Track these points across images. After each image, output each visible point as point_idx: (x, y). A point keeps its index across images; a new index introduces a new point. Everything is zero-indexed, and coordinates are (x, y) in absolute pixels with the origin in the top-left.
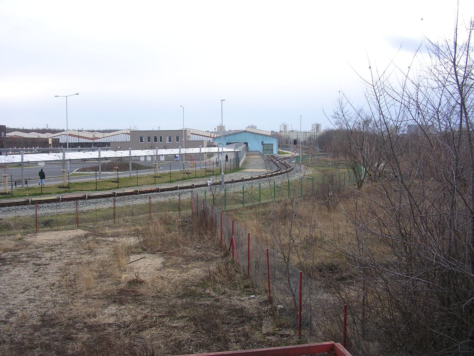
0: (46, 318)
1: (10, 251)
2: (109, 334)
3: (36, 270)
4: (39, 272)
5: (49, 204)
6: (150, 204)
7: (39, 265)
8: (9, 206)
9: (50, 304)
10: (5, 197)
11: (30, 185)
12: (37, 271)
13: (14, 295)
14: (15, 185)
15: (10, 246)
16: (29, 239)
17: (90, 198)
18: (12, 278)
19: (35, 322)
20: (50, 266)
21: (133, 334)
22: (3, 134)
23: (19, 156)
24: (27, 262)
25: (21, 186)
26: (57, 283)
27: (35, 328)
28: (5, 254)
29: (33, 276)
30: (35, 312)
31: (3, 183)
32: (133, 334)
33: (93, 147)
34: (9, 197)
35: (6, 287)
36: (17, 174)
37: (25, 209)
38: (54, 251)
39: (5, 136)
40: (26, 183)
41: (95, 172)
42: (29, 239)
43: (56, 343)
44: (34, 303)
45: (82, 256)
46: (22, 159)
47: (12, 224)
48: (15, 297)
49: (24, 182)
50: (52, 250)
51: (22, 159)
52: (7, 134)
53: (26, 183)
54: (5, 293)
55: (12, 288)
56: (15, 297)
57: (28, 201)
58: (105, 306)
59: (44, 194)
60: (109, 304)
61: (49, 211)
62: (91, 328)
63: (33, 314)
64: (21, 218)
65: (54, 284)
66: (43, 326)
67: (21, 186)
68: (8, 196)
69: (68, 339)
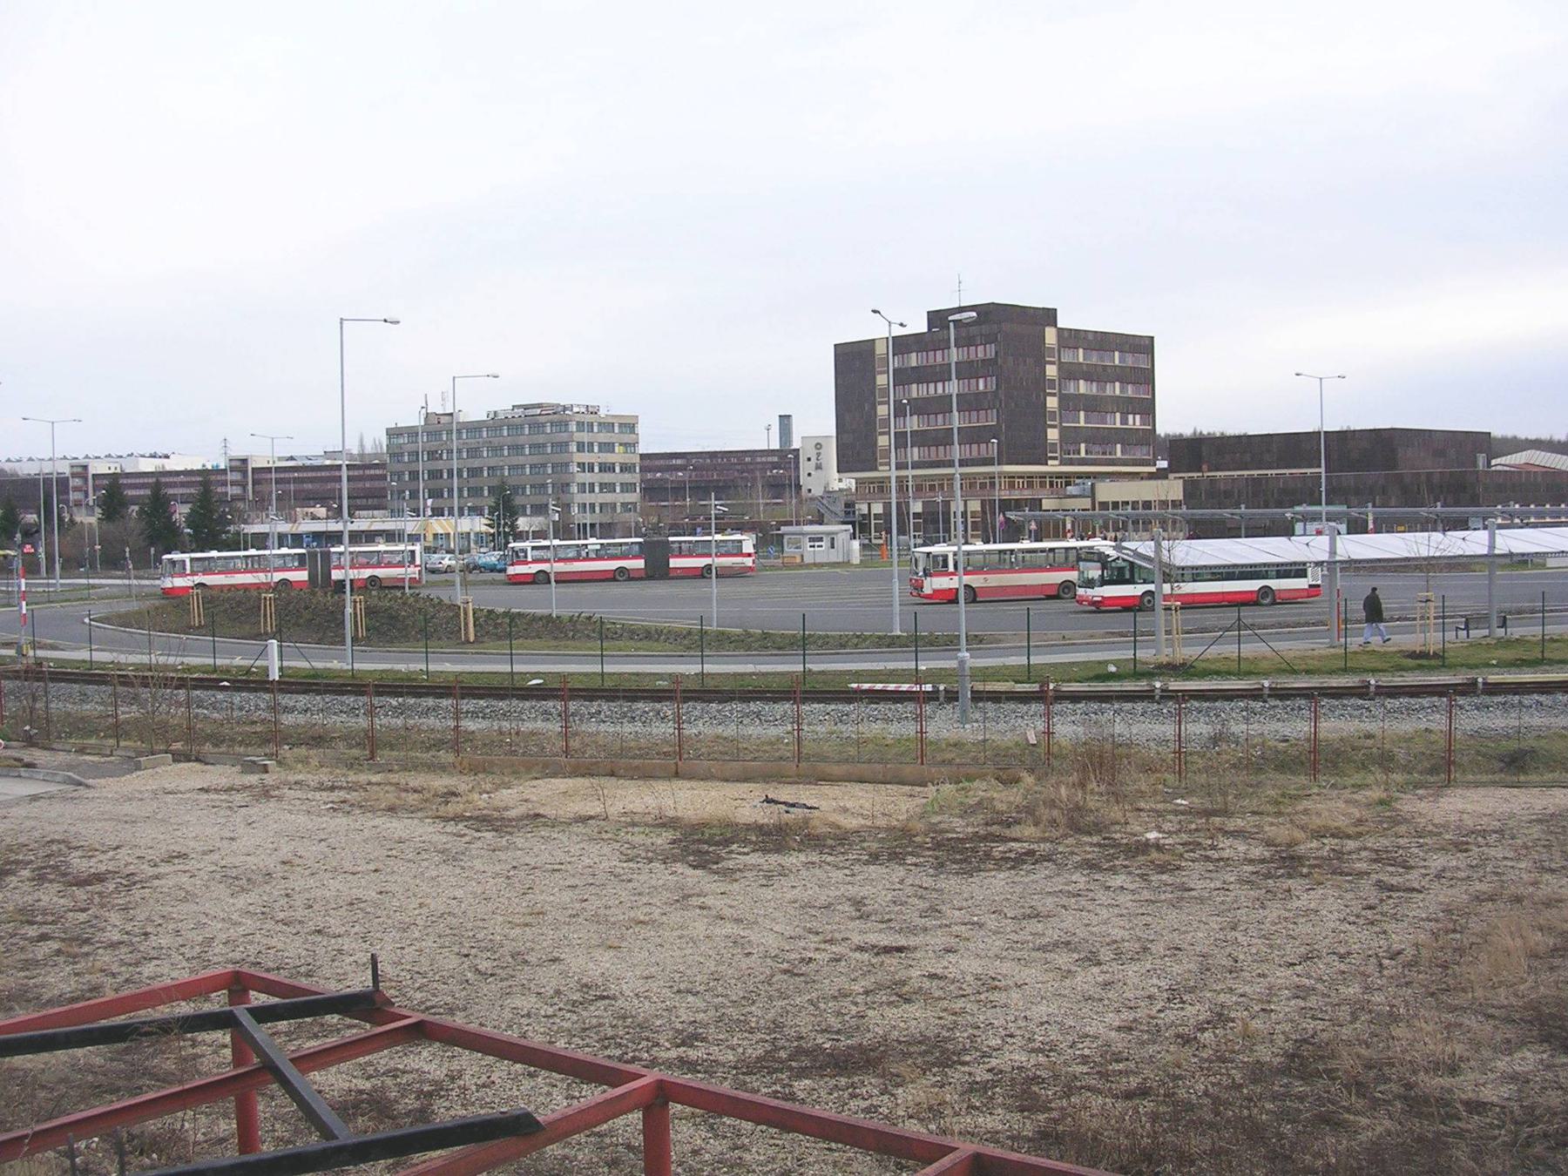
0: (1306, 1051)
1: (1333, 836)
2: (1460, 1134)
3: (1372, 901)
4: (1379, 909)
5: (1542, 698)
6: (1315, 739)
7: (1392, 888)
8: (1412, 695)
9: (1344, 1013)
10: (1420, 667)
11: (1516, 632)
12: (1370, 908)
13: (1264, 968)
14: (1467, 628)
15: (1341, 822)
16: (1409, 804)
17: (1493, 689)
18: (1286, 919)
19: (1264, 1053)
20: (1421, 896)
21: (1538, 1149)
22: (1481, 459)
23: (1483, 535)
24: (1361, 874)
25: (1486, 632)
26: (1410, 952)
27: (1258, 1072)
28: (1315, 844)
29: (1352, 919)
30: (1287, 1027)
31: (1419, 622)
32: (1538, 1149)
33: (1237, 571)
34: (1431, 669)
35: (1254, 941)
36: (1465, 594)
37: (1461, 708)
38: (1466, 851)
39: (1489, 465)
40: (1504, 624)
41: (1034, 660)
42: (1409, 804)
43: (1287, 1128)
44: (1304, 999)
45: (1547, 876)
46: (1492, 546)
47: (1401, 755)
48: (1259, 975)
49: (1495, 622)
50: (1461, 847)
51: (1492, 546)
52: (1493, 462)
53: (1504, 624)
54: (1241, 957)
55: (1271, 946)
56: (1259, 975)
57: (1474, 683)
58: (1509, 1047)
59: (1551, 662)
60: (1522, 1044)
61: (1536, 720)
62: (1416, 1103)
63: (1276, 1028)
64: (1433, 737)
65: (1399, 953)
66: (1284, 1071)
67: (1486, 632)
68: (1433, 662)
69: (1327, 1122)
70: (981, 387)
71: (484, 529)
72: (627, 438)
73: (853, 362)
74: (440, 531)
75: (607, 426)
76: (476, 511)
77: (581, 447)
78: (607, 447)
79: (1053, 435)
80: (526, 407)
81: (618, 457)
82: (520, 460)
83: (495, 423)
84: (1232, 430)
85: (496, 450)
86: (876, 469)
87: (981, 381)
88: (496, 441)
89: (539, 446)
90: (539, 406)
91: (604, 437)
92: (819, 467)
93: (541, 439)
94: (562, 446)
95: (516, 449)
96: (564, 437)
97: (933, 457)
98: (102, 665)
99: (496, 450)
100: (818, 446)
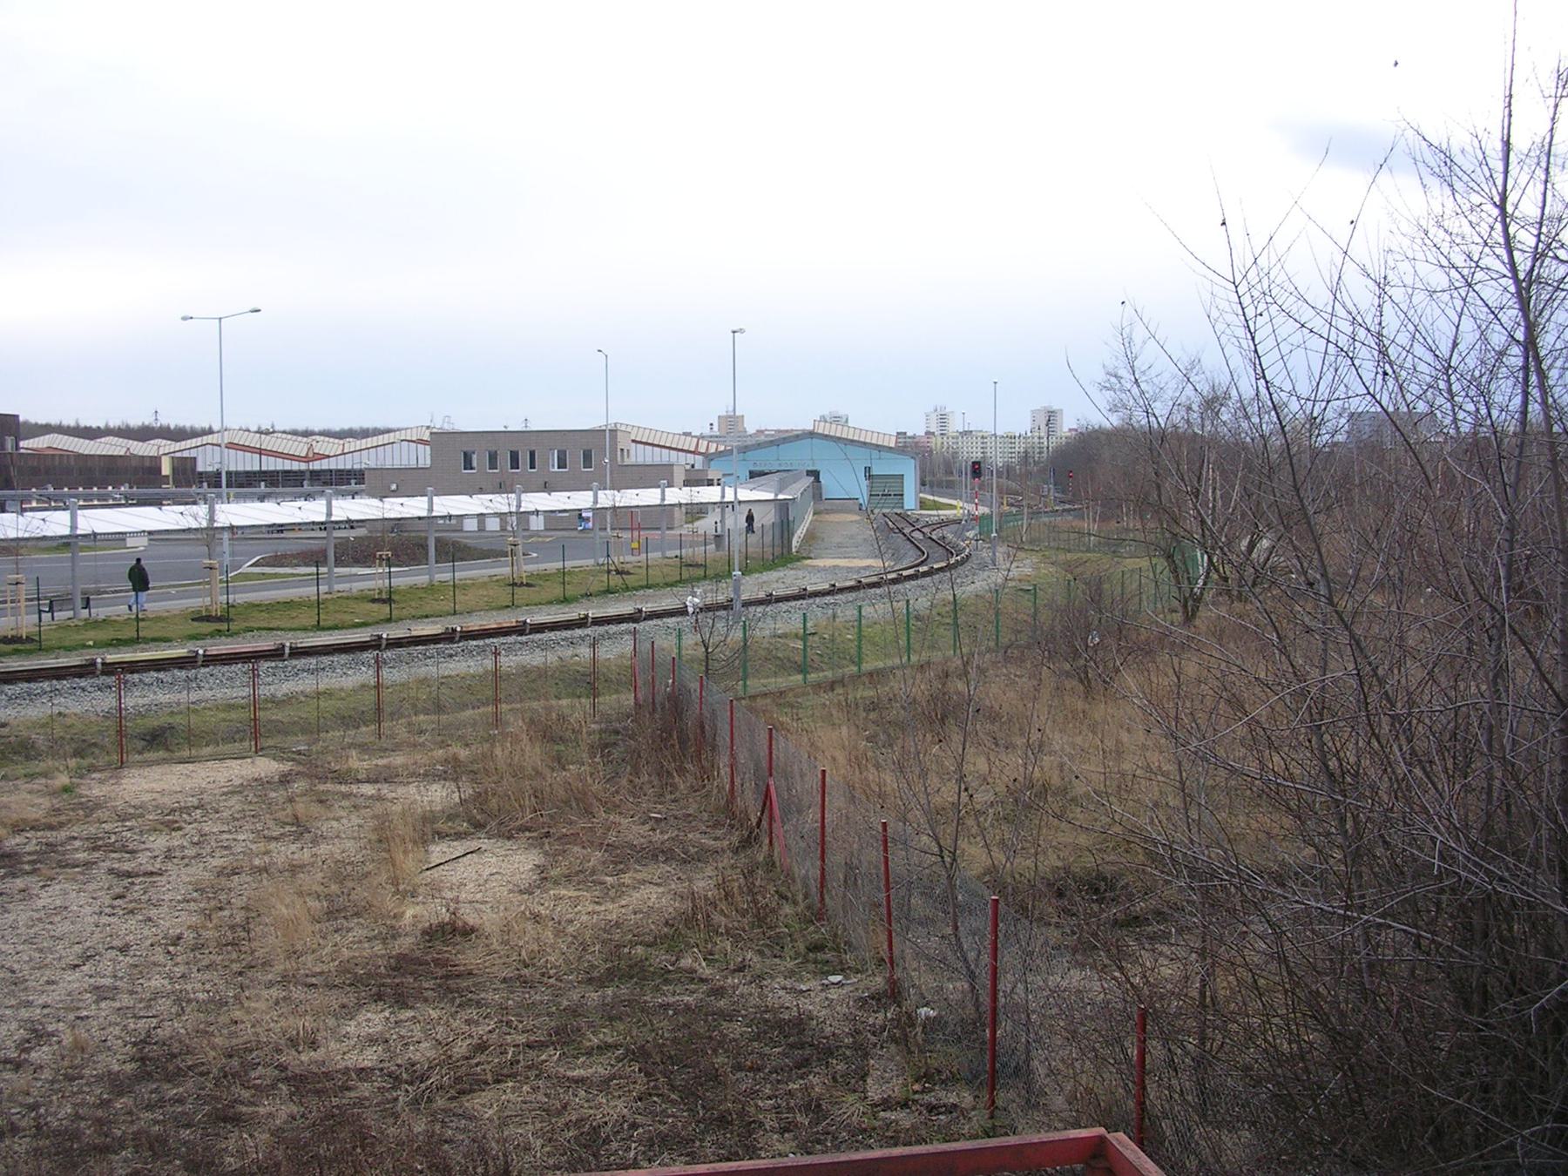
0: (152, 1051)
1: (32, 828)
2: (360, 1103)
3: (118, 890)
4: (129, 897)
5: (161, 675)
6: (496, 674)
7: (129, 875)
8: (28, 680)
9: (164, 1006)
10: (17, 652)
11: (99, 612)
12: (121, 897)
13: (48, 974)
14: (51, 610)
15: (33, 814)
16: (95, 789)
17: (298, 653)
18: (40, 920)
19: (115, 1063)
20: (164, 879)
21: (440, 1102)
22: (9, 442)
23: (64, 517)
24: (88, 864)
25: (71, 614)
26: (189, 936)
27: (117, 1085)
28: (18, 839)
29: (108, 910)
30: (117, 1031)
31: (9, 605)
32: (440, 1102)
34: (29, 652)
35: (20, 948)
36: (55, 574)
37: (83, 690)
38: (180, 829)
39: (17, 448)
40: (87, 605)
42: (95, 789)
43: (185, 1134)
44: (113, 999)
45: (273, 845)
46: (74, 526)
47: (41, 741)
48: (48, 983)
49: (79, 603)
50: (172, 827)
51: (74, 526)
52: (22, 444)
53: (87, 605)
54: (16, 966)
55: (41, 951)
56: (48, 983)
57: (93, 663)
58: (347, 1012)
59: (147, 641)
60: (359, 1006)
61: (163, 697)
62: (300, 1083)
63: (110, 1037)
64: (69, 721)
65: (179, 938)
66: (143, 1076)
67: (71, 614)
68: (28, 646)
69: (225, 1120)
98: (51, 503)
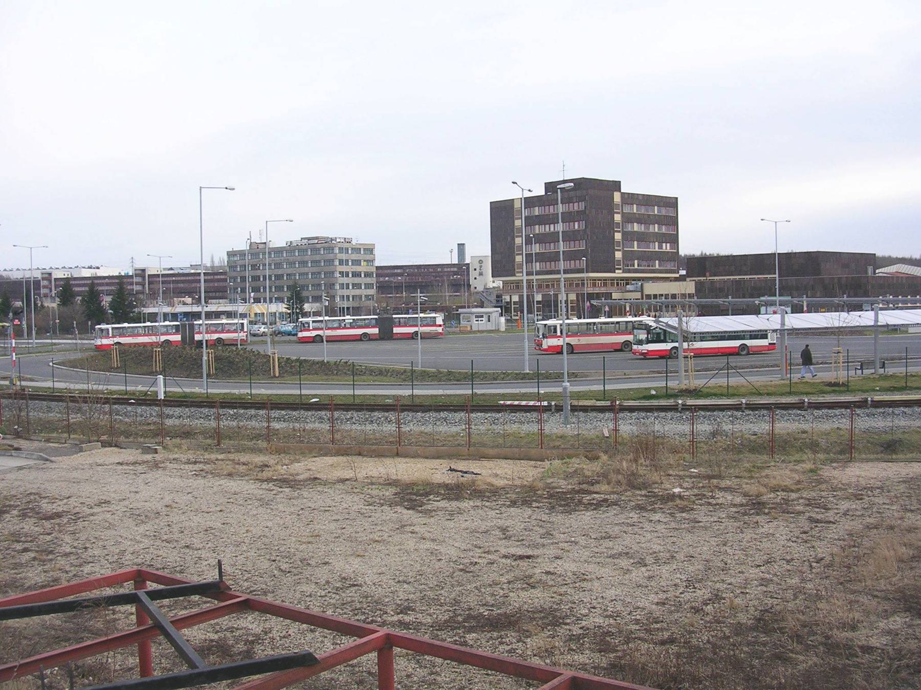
0: (767, 616)
1: (783, 490)
2: (857, 666)
3: (806, 529)
4: (810, 533)
5: (906, 410)
6: (772, 434)
7: (817, 521)
8: (829, 408)
9: (789, 594)
10: (834, 391)
11: (890, 371)
12: (805, 533)
13: (743, 568)
14: (862, 369)
15: (788, 482)
16: (828, 472)
17: (877, 404)
18: (755, 539)
19: (743, 618)
20: (835, 526)
21: (903, 674)
22: (870, 269)
23: (871, 314)
24: (799, 513)
25: (873, 371)
26: (828, 559)
27: (739, 629)
28: (772, 495)
29: (794, 539)
30: (756, 603)
31: (833, 365)
32: (903, 674)
33: (726, 335)
34: (841, 392)
35: (737, 552)
36: (861, 349)
37: (858, 415)
38: (861, 499)
39: (875, 273)
40: (883, 366)
41: (607, 387)
42: (828, 472)
43: (756, 662)
44: (766, 586)
45: (909, 514)
46: (876, 320)
47: (823, 443)
48: (740, 572)
49: (878, 365)
50: (858, 497)
51: (876, 320)
52: (877, 271)
53: (883, 366)
54: (729, 561)
55: (746, 555)
56: (740, 572)
57: (866, 401)
58: (886, 615)
59: (911, 388)
60: (894, 613)
61: (902, 422)
62: (832, 647)
63: (749, 603)
64: (842, 433)
65: (822, 559)
66: (754, 628)
67: (873, 371)
68: (842, 389)
69: (779, 658)
70: (576, 227)
71: (284, 310)
72: (368, 257)
73: (501, 213)
74: (259, 312)
75: (357, 250)
76: (280, 300)
77: (341, 262)
78: (357, 262)
79: (618, 255)
80: (309, 239)
81: (363, 268)
82: (306, 270)
83: (291, 248)
84: (723, 253)
85: (291, 264)
86: (514, 275)
87: (576, 224)
88: (291, 259)
89: (316, 262)
90: (317, 238)
91: (355, 257)
92: (481, 274)
93: (317, 258)
94: (330, 262)
95: (303, 263)
96: (331, 256)
97: (548, 268)
98: (60, 390)
99: (291, 264)
100: (481, 262)
